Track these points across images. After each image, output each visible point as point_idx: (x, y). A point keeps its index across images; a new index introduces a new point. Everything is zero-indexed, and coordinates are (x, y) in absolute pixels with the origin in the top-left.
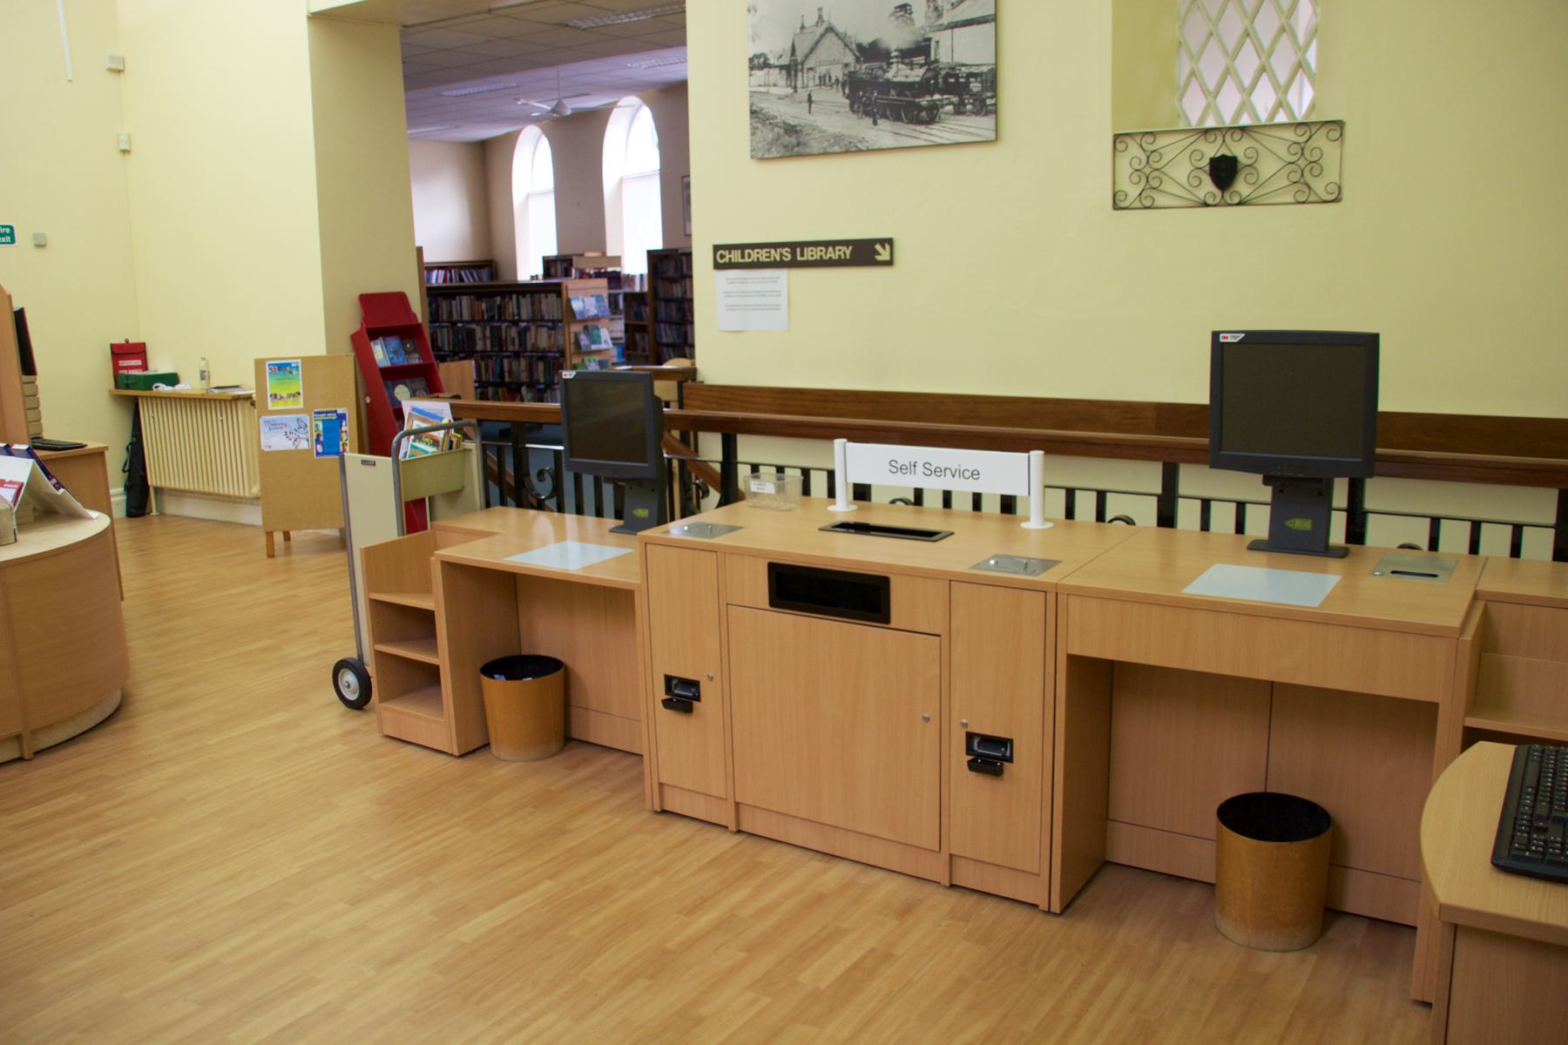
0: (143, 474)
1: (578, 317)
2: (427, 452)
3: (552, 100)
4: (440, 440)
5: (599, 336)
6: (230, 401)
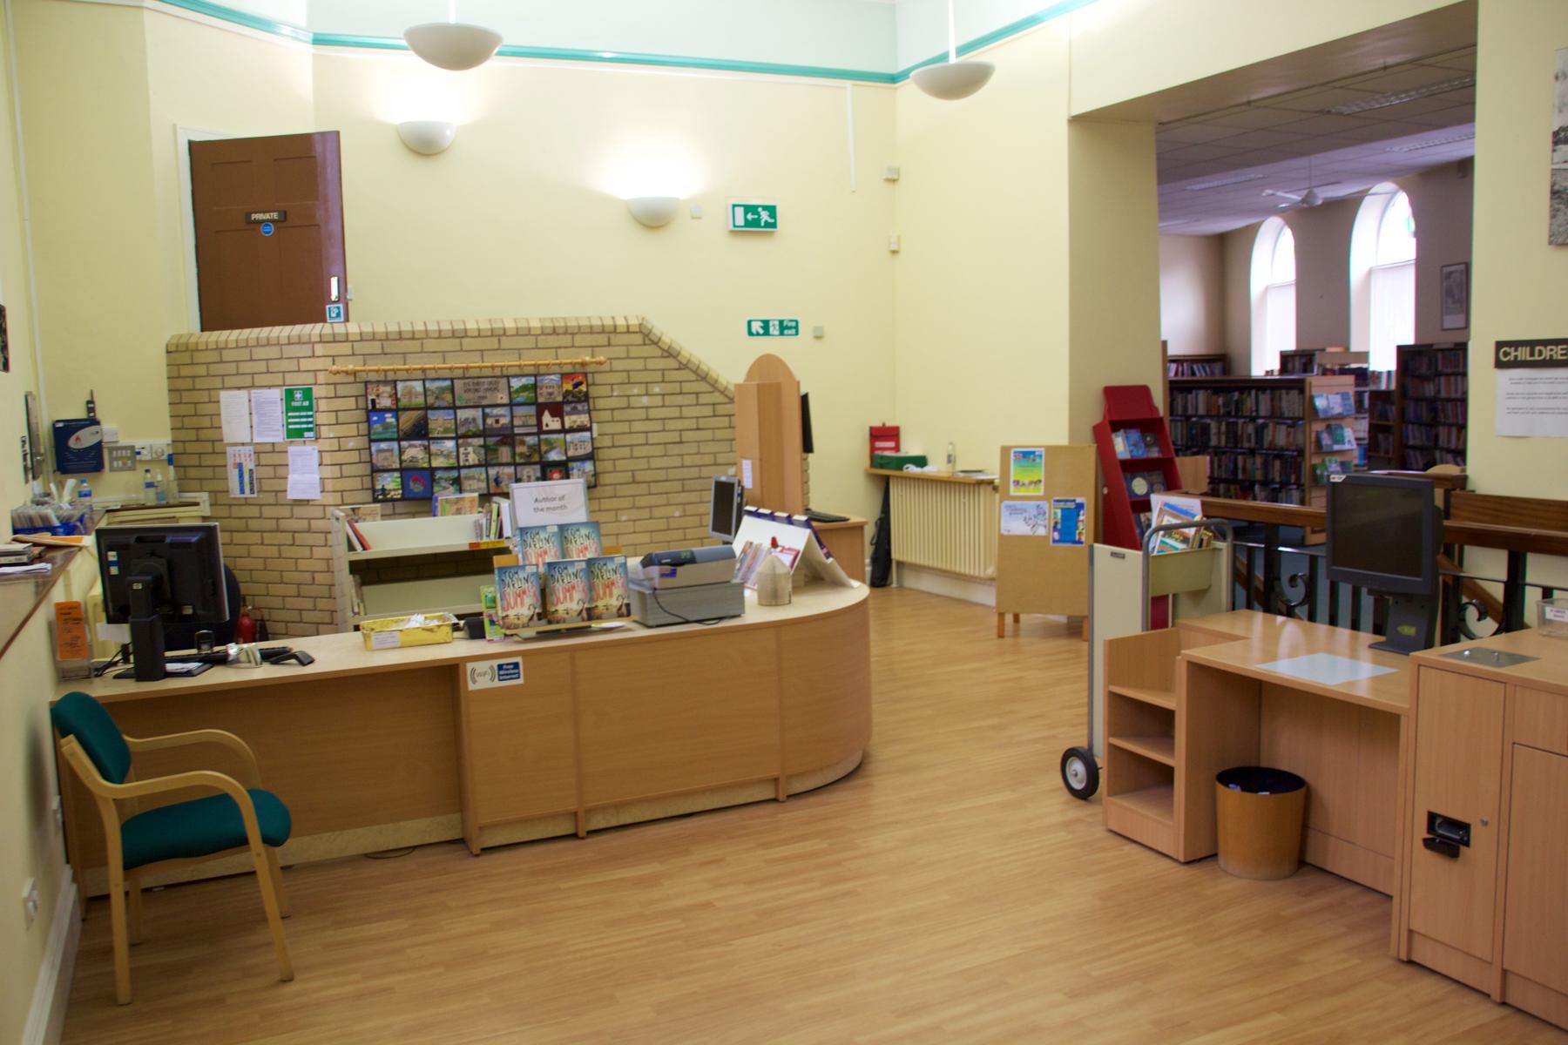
0: (887, 547)
1: (1321, 416)
2: (1177, 549)
3: (1305, 189)
4: (1191, 537)
5: (1343, 436)
6: (974, 484)
